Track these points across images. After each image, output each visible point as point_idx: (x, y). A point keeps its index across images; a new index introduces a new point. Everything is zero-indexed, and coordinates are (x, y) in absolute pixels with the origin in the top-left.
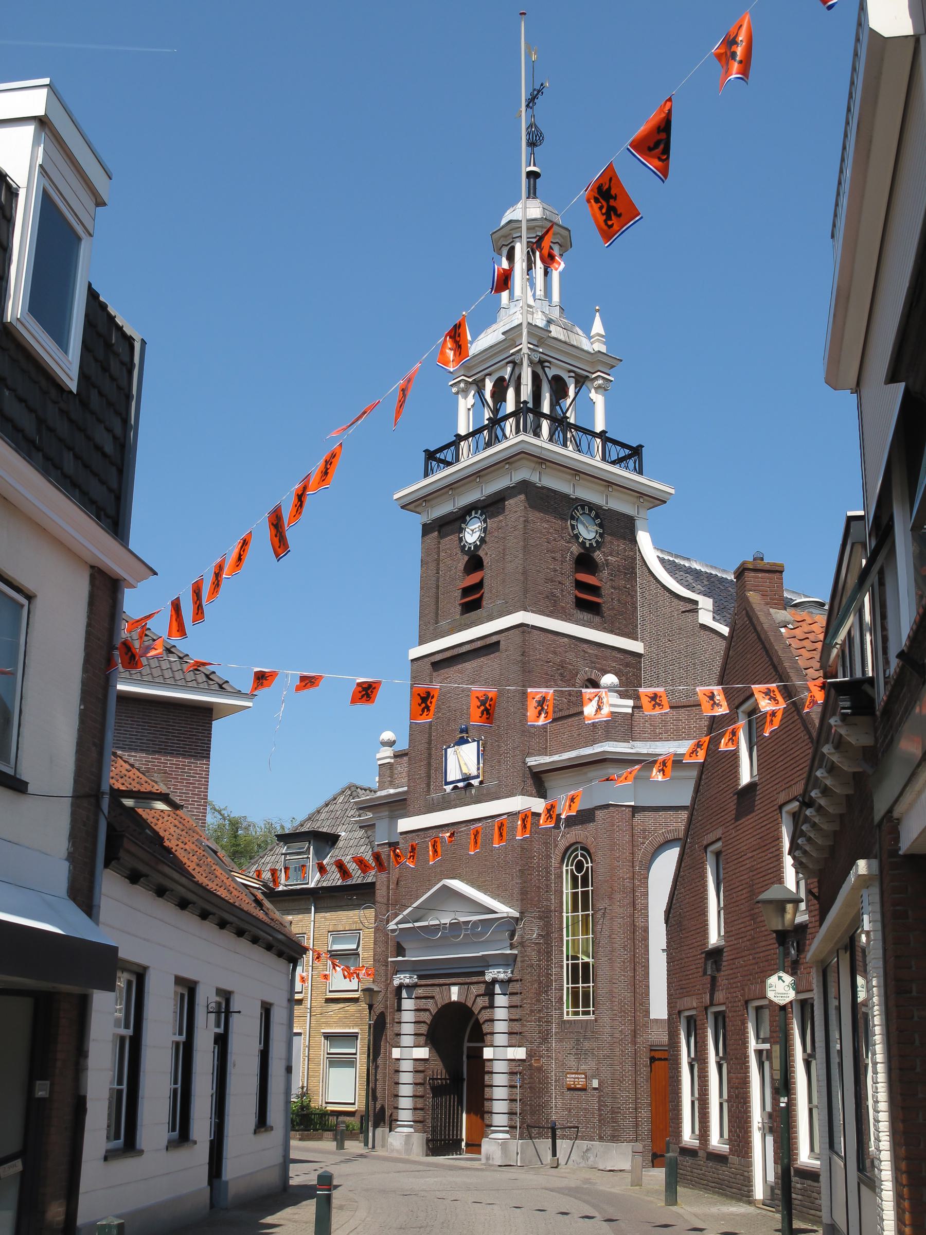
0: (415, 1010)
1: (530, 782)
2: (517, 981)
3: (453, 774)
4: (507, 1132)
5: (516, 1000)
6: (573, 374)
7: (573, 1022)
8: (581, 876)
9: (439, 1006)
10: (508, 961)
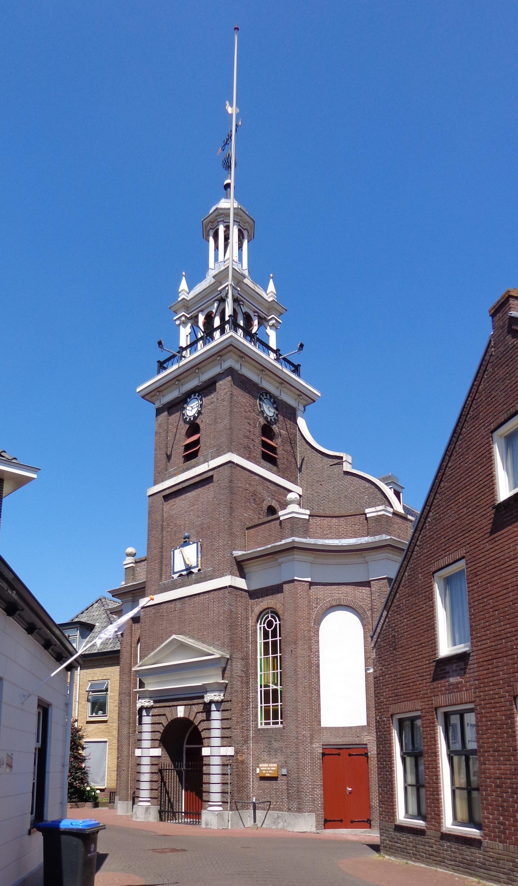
0: (152, 724)
1: (235, 567)
2: (228, 701)
3: (179, 566)
4: (220, 806)
5: (227, 714)
6: (256, 314)
7: (266, 730)
8: (271, 631)
9: (169, 720)
10: (224, 688)
